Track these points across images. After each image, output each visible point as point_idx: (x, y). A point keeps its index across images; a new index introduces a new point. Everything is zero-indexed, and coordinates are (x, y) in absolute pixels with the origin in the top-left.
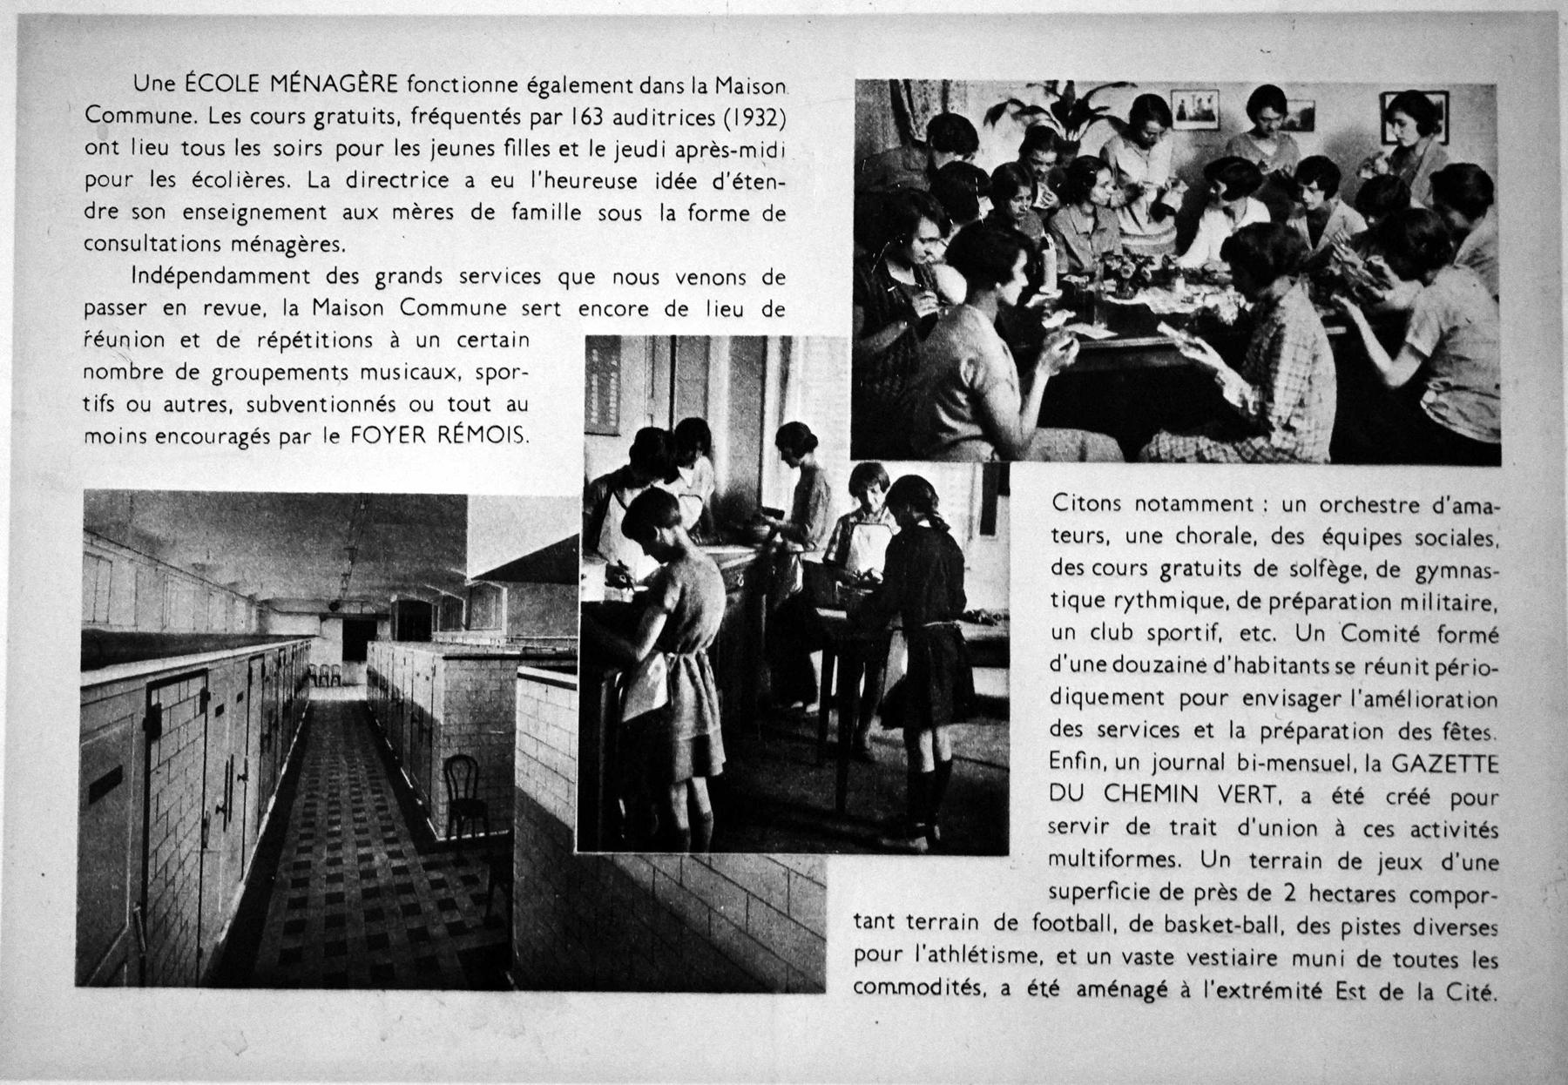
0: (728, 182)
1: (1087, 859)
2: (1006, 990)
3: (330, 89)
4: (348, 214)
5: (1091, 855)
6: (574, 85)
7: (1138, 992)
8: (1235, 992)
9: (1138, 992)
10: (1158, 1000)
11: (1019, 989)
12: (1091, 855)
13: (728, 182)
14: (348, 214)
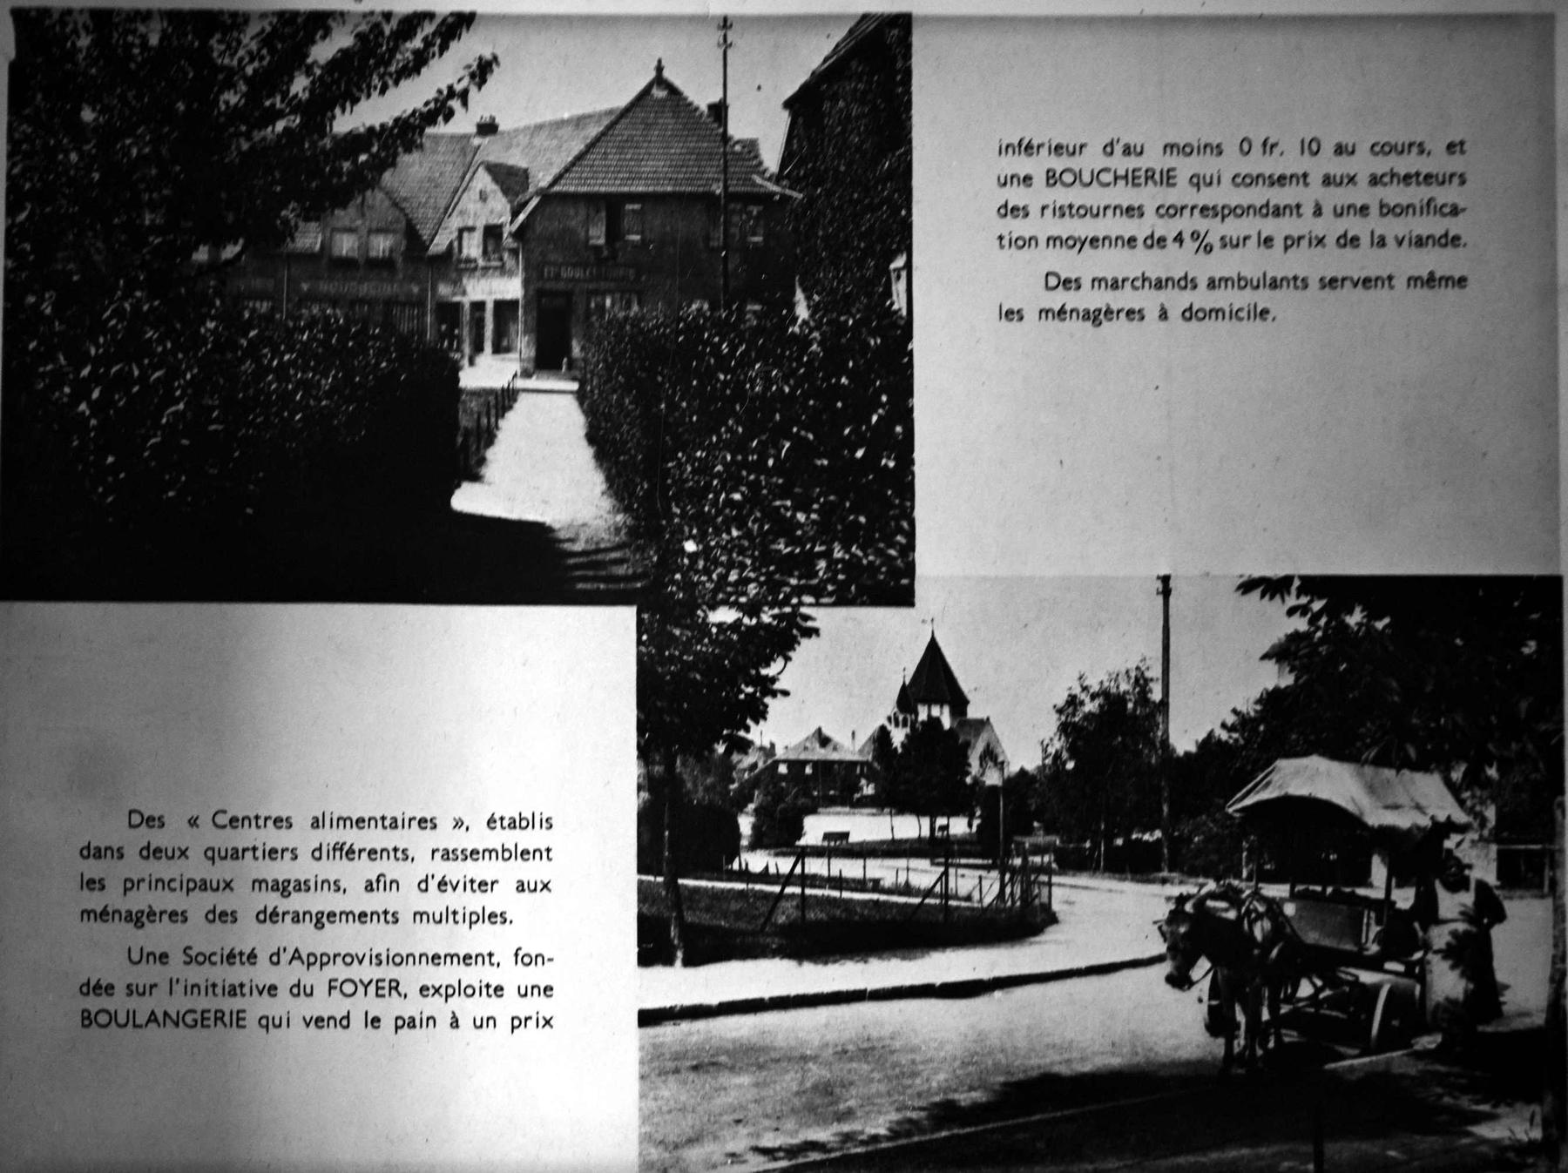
0: (433, 884)
1: (451, 917)
2: (1164, 315)
3: (152, 1025)
4: (521, 887)
5: (455, 913)
6: (525, 852)
7: (1086, 315)
8: (437, 991)
9: (1086, 315)
10: (1105, 324)
11: (1175, 314)
12: (455, 913)
13: (433, 884)
14: (521, 887)
